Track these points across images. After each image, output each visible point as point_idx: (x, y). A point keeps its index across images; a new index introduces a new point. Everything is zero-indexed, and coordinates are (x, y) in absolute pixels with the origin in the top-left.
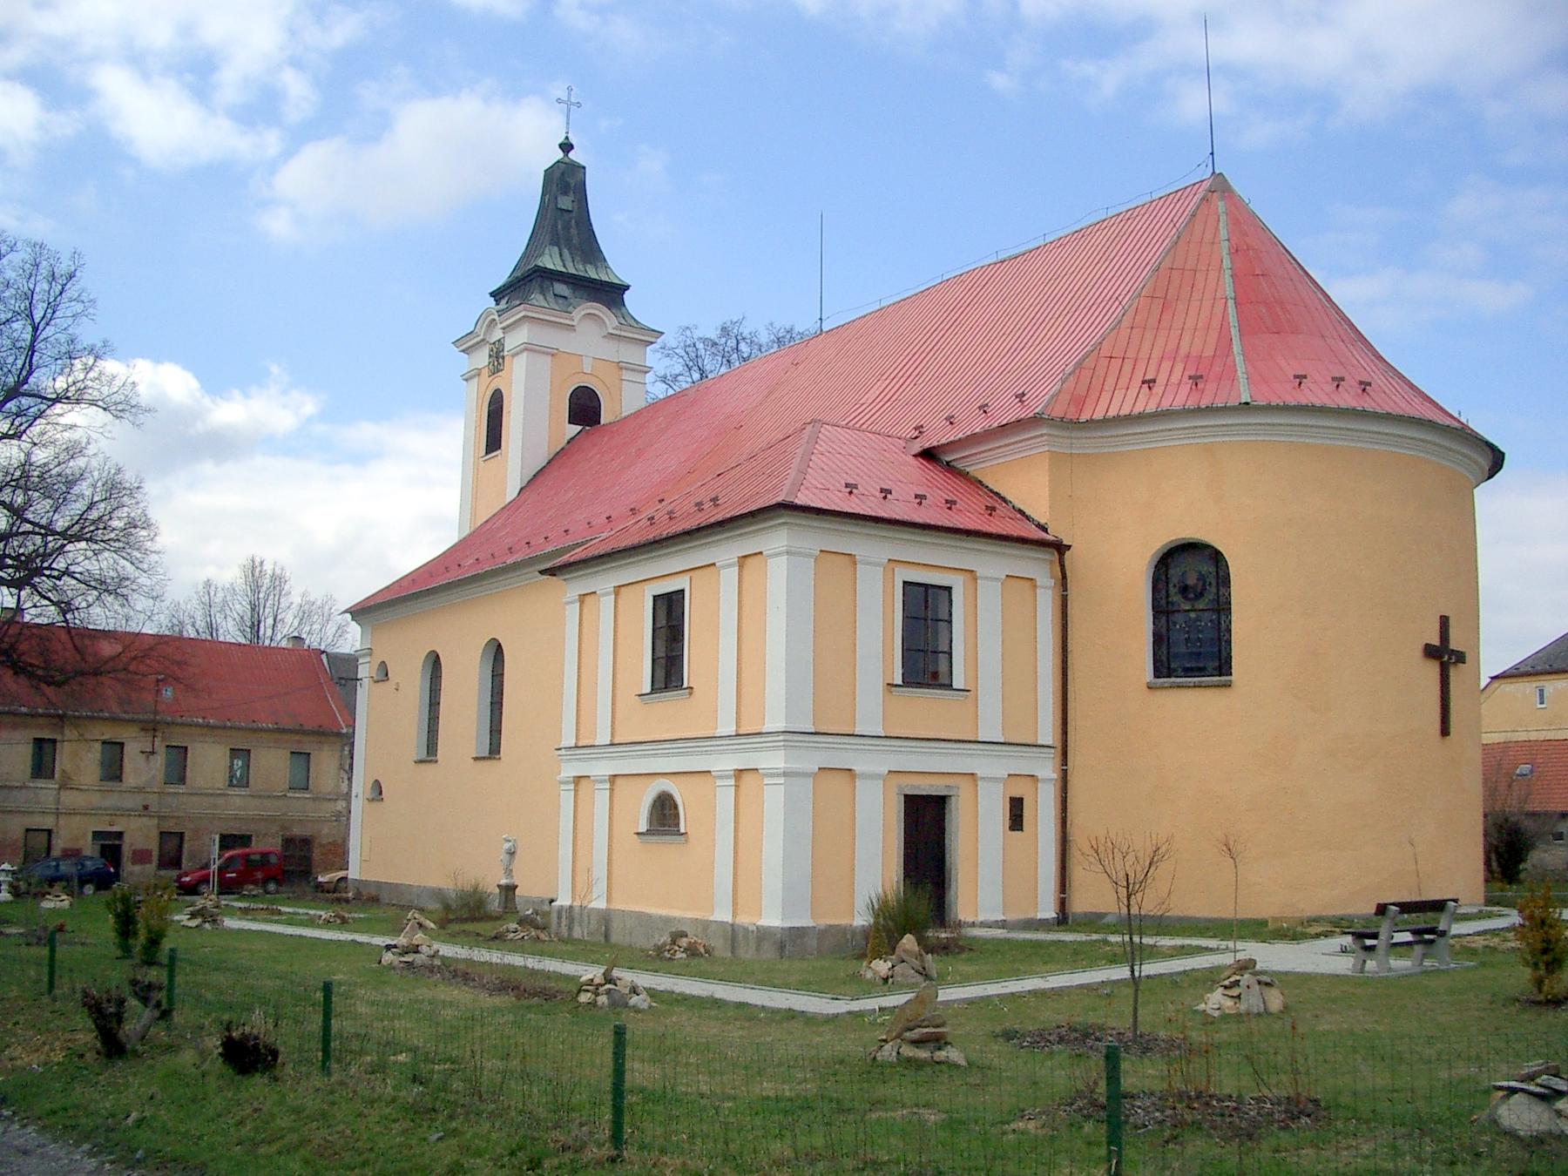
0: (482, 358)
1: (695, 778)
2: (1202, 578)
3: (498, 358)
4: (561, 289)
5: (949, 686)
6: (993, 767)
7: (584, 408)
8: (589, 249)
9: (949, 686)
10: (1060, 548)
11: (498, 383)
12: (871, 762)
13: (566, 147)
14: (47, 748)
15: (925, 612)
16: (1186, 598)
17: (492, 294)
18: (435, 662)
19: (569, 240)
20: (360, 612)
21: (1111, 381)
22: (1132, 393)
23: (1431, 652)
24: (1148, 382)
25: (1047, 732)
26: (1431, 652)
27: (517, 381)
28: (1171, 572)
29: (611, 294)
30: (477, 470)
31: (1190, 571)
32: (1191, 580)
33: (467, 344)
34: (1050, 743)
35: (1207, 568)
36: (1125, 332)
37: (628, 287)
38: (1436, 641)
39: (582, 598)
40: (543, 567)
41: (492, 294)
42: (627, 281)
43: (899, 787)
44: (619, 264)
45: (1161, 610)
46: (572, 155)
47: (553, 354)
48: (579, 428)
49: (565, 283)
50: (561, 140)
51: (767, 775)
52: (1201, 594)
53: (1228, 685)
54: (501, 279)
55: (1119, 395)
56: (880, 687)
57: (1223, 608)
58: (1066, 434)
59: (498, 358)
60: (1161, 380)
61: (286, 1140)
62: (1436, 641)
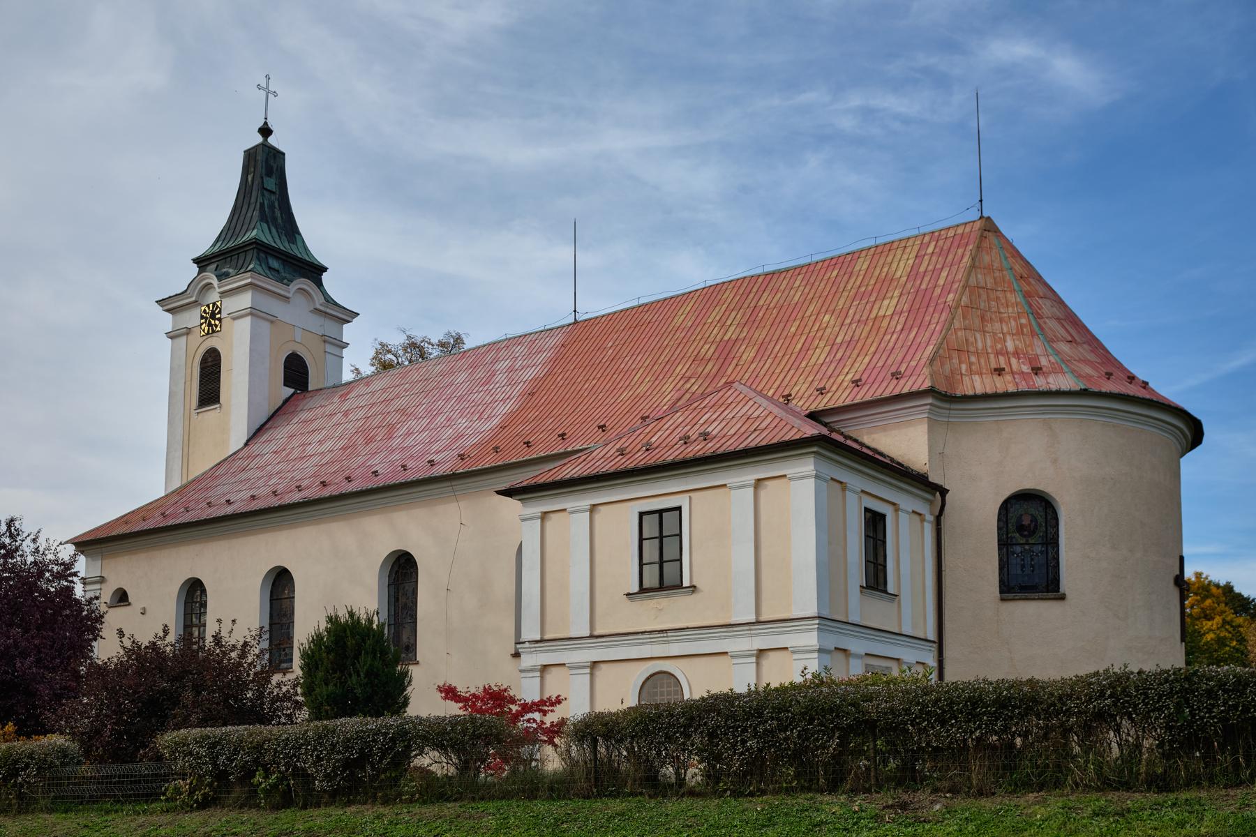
0: (192, 318)
2: (1034, 519)
3: (212, 317)
4: (275, 264)
7: (296, 372)
8: (290, 229)
11: (213, 342)
13: (266, 131)
14: (651, 579)
16: (1022, 535)
17: (197, 261)
19: (274, 219)
20: (85, 544)
27: (238, 345)
28: (1010, 515)
29: (315, 271)
31: (1027, 513)
32: (1026, 521)
33: (171, 305)
34: (932, 639)
35: (1036, 510)
37: (325, 269)
39: (593, 508)
40: (502, 487)
41: (197, 261)
42: (325, 264)
45: (1004, 544)
46: (271, 140)
47: (272, 320)
48: (291, 391)
49: (277, 258)
50: (261, 124)
51: (794, 652)
52: (1034, 532)
54: (204, 245)
57: (1052, 542)
58: (947, 406)
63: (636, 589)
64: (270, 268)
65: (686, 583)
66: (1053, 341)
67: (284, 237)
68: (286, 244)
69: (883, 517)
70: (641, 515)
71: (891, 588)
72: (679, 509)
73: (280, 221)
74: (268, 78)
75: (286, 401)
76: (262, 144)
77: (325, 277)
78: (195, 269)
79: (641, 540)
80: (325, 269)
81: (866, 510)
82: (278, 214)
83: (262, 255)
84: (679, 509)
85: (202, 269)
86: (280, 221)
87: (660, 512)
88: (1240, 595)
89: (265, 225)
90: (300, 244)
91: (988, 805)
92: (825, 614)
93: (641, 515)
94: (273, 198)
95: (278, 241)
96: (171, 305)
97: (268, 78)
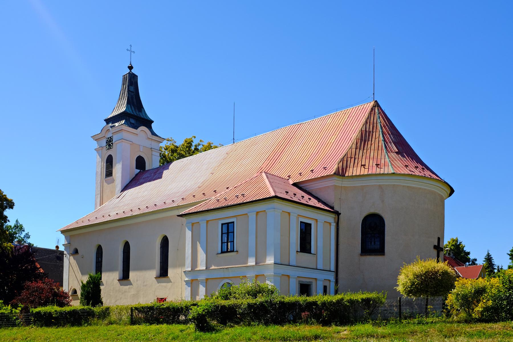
1: (302, 265)
5: (310, 253)
6: (321, 276)
9: (310, 253)
10: (338, 214)
11: (110, 152)
12: (294, 273)
13: (131, 68)
15: (306, 231)
17: (105, 120)
18: (99, 250)
21: (352, 164)
22: (359, 168)
23: (435, 247)
24: (363, 165)
25: (333, 268)
26: (435, 247)
29: (148, 123)
30: (102, 187)
33: (96, 138)
36: (354, 150)
37: (153, 122)
38: (436, 244)
41: (105, 120)
43: (299, 281)
44: (150, 111)
46: (133, 71)
53: (384, 255)
55: (355, 169)
56: (295, 252)
59: (110, 143)
60: (367, 164)
61: (393, 330)
62: (436, 244)
63: (220, 251)
64: (131, 123)
65: (235, 250)
66: (389, 152)
67: (137, 110)
68: (138, 113)
69: (310, 224)
70: (222, 224)
71: (313, 251)
72: (233, 222)
73: (135, 103)
74: (131, 46)
75: (137, 175)
76: (129, 73)
77: (153, 125)
78: (105, 123)
79: (222, 234)
80: (153, 122)
81: (301, 222)
82: (135, 100)
83: (128, 118)
84: (233, 222)
85: (108, 123)
86: (135, 103)
87: (228, 224)
88: (100, 291)
89: (129, 106)
90: (143, 112)
91: (497, 326)
92: (279, 261)
93: (222, 224)
94: (133, 94)
95: (134, 112)
96: (96, 138)
97: (131, 46)
